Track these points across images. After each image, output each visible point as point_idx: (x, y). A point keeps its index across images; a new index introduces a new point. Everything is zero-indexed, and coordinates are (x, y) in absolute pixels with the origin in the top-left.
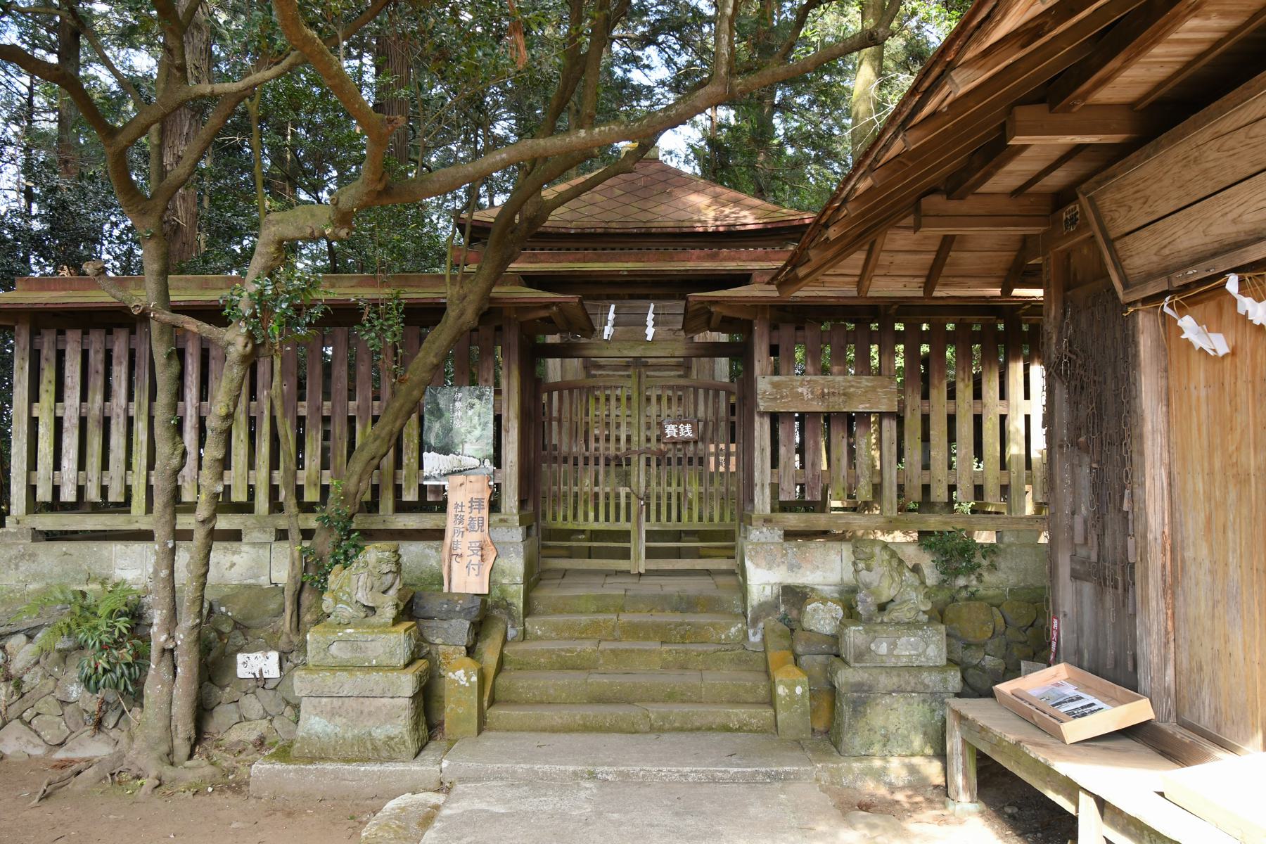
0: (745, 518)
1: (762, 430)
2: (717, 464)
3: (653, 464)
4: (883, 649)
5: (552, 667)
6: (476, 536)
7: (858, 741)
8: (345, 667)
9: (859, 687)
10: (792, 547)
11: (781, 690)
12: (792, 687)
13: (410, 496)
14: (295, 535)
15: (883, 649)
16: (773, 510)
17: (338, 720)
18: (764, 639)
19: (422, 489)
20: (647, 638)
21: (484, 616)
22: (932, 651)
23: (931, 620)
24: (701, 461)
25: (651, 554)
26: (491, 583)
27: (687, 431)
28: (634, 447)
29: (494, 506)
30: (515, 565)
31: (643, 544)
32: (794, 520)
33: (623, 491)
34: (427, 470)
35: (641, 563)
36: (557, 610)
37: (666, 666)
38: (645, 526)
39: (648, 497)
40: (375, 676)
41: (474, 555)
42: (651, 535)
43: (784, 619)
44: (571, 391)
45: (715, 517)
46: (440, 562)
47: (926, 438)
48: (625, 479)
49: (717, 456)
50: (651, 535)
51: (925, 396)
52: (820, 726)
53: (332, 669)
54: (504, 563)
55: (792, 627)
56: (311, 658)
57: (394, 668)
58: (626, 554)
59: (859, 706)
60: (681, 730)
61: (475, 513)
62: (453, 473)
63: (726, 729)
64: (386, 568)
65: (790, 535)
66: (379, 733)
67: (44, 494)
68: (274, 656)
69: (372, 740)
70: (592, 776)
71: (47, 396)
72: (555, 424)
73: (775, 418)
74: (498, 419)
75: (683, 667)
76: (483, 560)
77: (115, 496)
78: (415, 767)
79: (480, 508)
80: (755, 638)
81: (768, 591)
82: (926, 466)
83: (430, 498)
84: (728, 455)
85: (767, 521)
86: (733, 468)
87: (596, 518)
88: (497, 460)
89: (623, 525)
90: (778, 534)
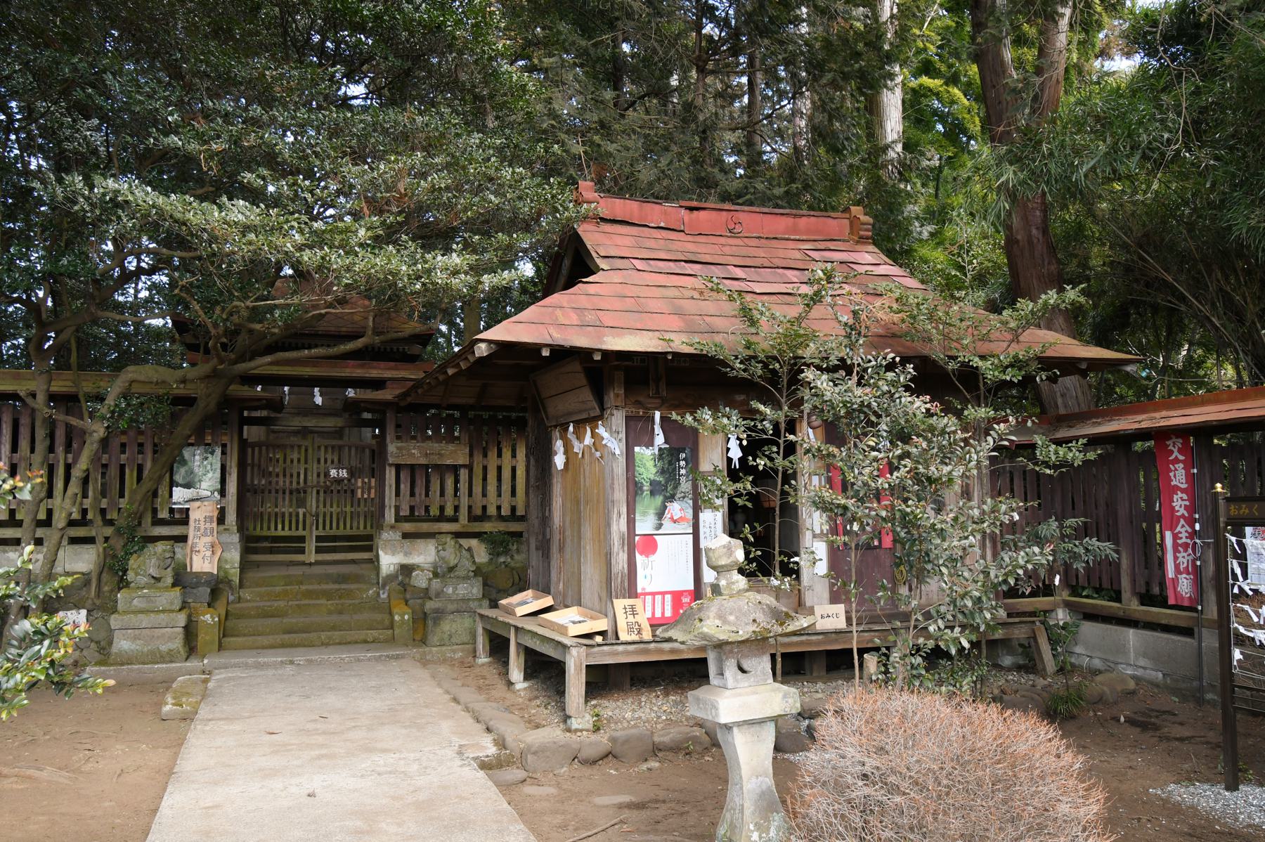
0: (380, 527)
1: (390, 475)
2: (363, 493)
3: (322, 494)
4: (450, 590)
5: (259, 616)
6: (208, 539)
7: (436, 638)
8: (141, 612)
9: (437, 611)
10: (407, 543)
11: (397, 618)
12: (402, 616)
13: (164, 514)
14: (100, 540)
15: (450, 590)
16: (396, 521)
17: (138, 642)
18: (389, 596)
19: (172, 511)
20: (317, 598)
21: (216, 587)
22: (475, 591)
23: (475, 575)
24: (353, 491)
25: (319, 550)
26: (219, 568)
27: (344, 473)
28: (309, 483)
29: (221, 520)
30: (235, 556)
31: (314, 544)
32: (408, 527)
33: (301, 511)
34: (175, 499)
35: (312, 557)
36: (258, 585)
37: (330, 613)
38: (315, 533)
39: (317, 515)
40: (162, 616)
41: (208, 552)
42: (319, 539)
43: (402, 584)
44: (267, 447)
45: (360, 528)
46: (185, 556)
47: (485, 479)
48: (302, 503)
49: (363, 488)
50: (319, 539)
51: (485, 456)
52: (418, 637)
53: (134, 612)
54: (227, 555)
55: (404, 587)
56: (120, 606)
57: (172, 611)
58: (302, 551)
59: (437, 621)
60: (340, 644)
61: (208, 525)
62: (193, 500)
63: (365, 642)
64: (168, 555)
65: (406, 536)
66: (164, 648)
67: (405, 512)
68: (84, 612)
69: (160, 652)
70: (292, 662)
72: (249, 469)
73: (398, 468)
74: (223, 468)
75: (340, 613)
76: (213, 552)
78: (188, 664)
79: (211, 522)
80: (384, 596)
81: (392, 568)
82: (484, 495)
83: (177, 516)
84: (370, 488)
85: (392, 527)
86: (372, 496)
87: (283, 529)
88: (223, 492)
89: (301, 532)
90: (398, 536)
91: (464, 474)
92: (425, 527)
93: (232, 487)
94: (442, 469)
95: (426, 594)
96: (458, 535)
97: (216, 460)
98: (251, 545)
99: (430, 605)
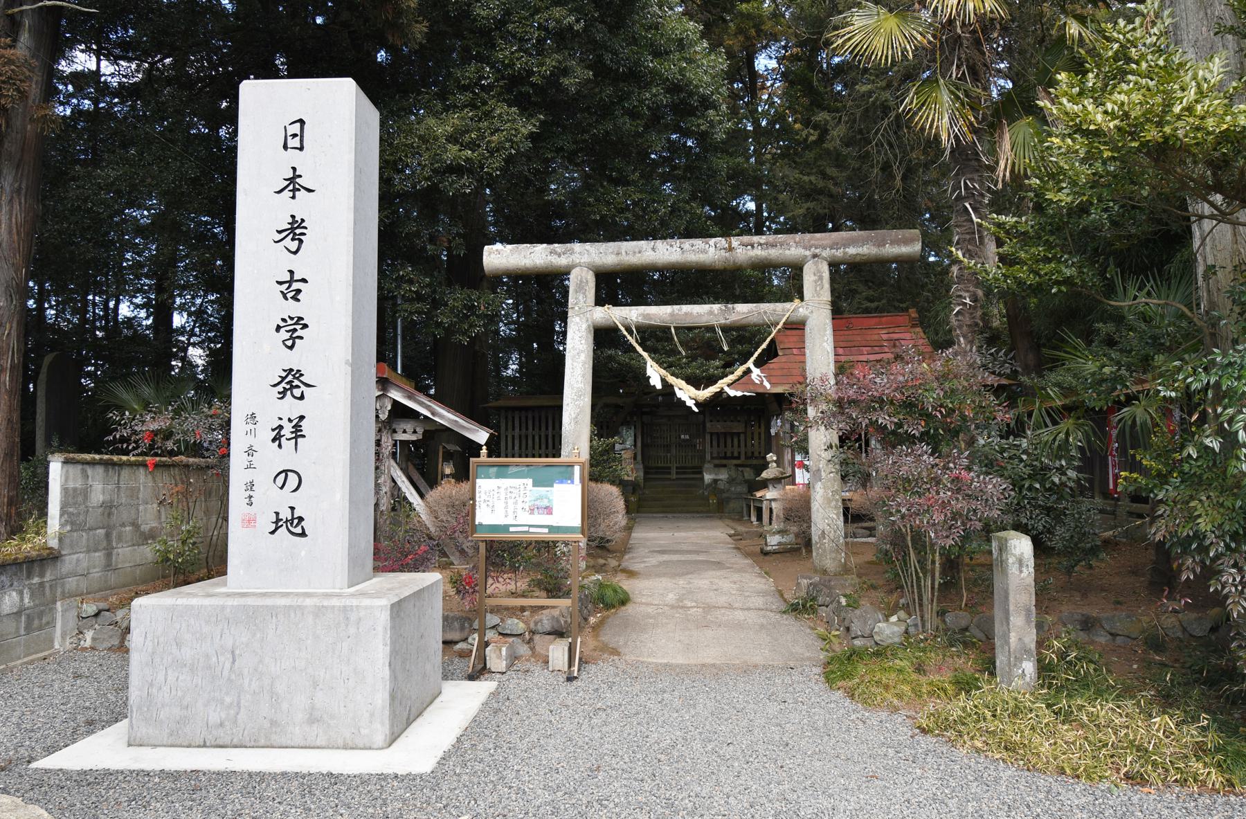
12: (713, 501)
29: (635, 458)
30: (641, 474)
32: (717, 462)
48: (669, 451)
65: (716, 466)
71: (543, 428)
73: (712, 434)
77: (736, 454)
91: (742, 437)
92: (724, 462)
93: (639, 444)
94: (732, 435)
95: (723, 491)
96: (737, 466)
97: (632, 432)
98: (647, 470)
99: (725, 495)
